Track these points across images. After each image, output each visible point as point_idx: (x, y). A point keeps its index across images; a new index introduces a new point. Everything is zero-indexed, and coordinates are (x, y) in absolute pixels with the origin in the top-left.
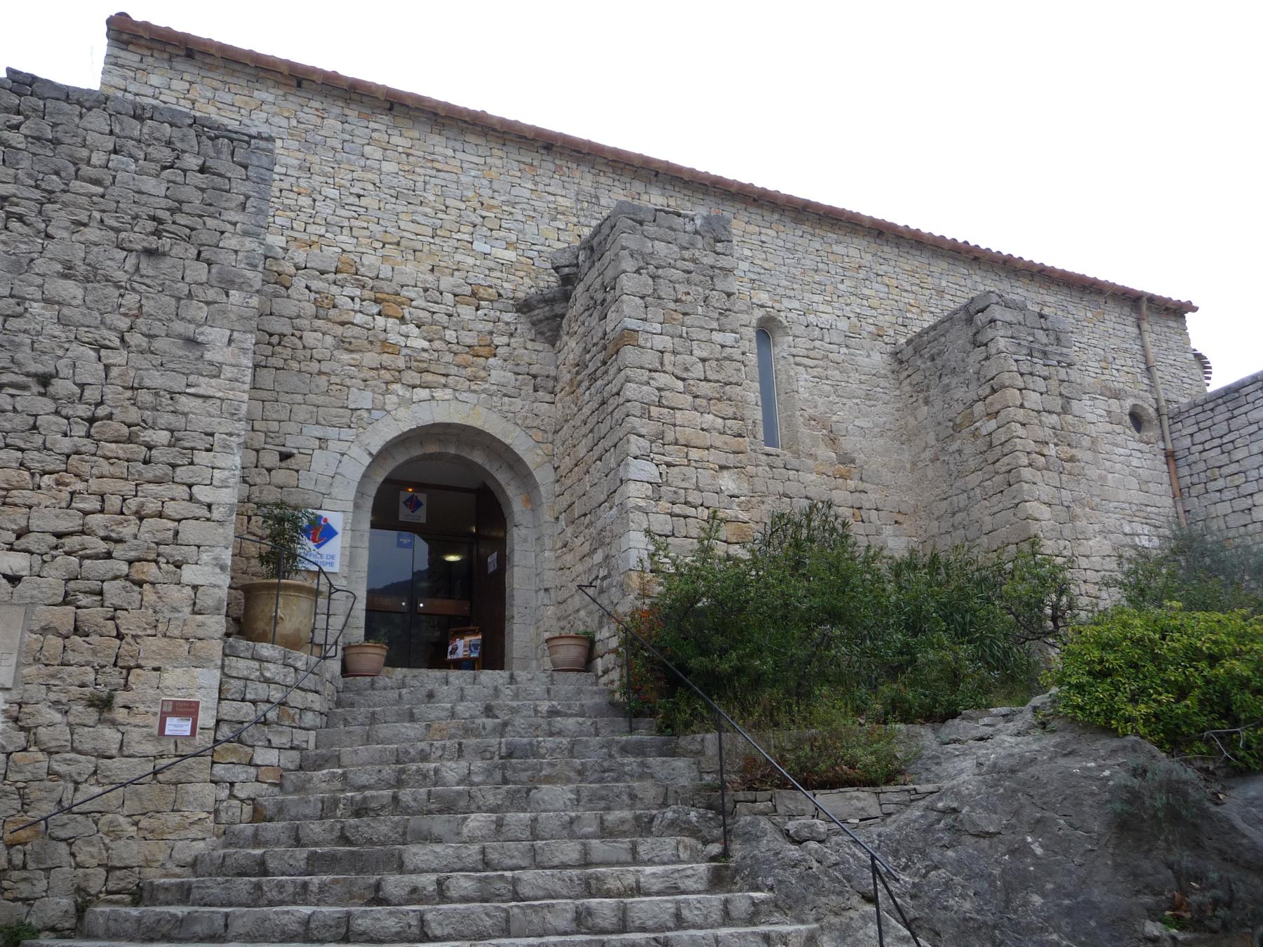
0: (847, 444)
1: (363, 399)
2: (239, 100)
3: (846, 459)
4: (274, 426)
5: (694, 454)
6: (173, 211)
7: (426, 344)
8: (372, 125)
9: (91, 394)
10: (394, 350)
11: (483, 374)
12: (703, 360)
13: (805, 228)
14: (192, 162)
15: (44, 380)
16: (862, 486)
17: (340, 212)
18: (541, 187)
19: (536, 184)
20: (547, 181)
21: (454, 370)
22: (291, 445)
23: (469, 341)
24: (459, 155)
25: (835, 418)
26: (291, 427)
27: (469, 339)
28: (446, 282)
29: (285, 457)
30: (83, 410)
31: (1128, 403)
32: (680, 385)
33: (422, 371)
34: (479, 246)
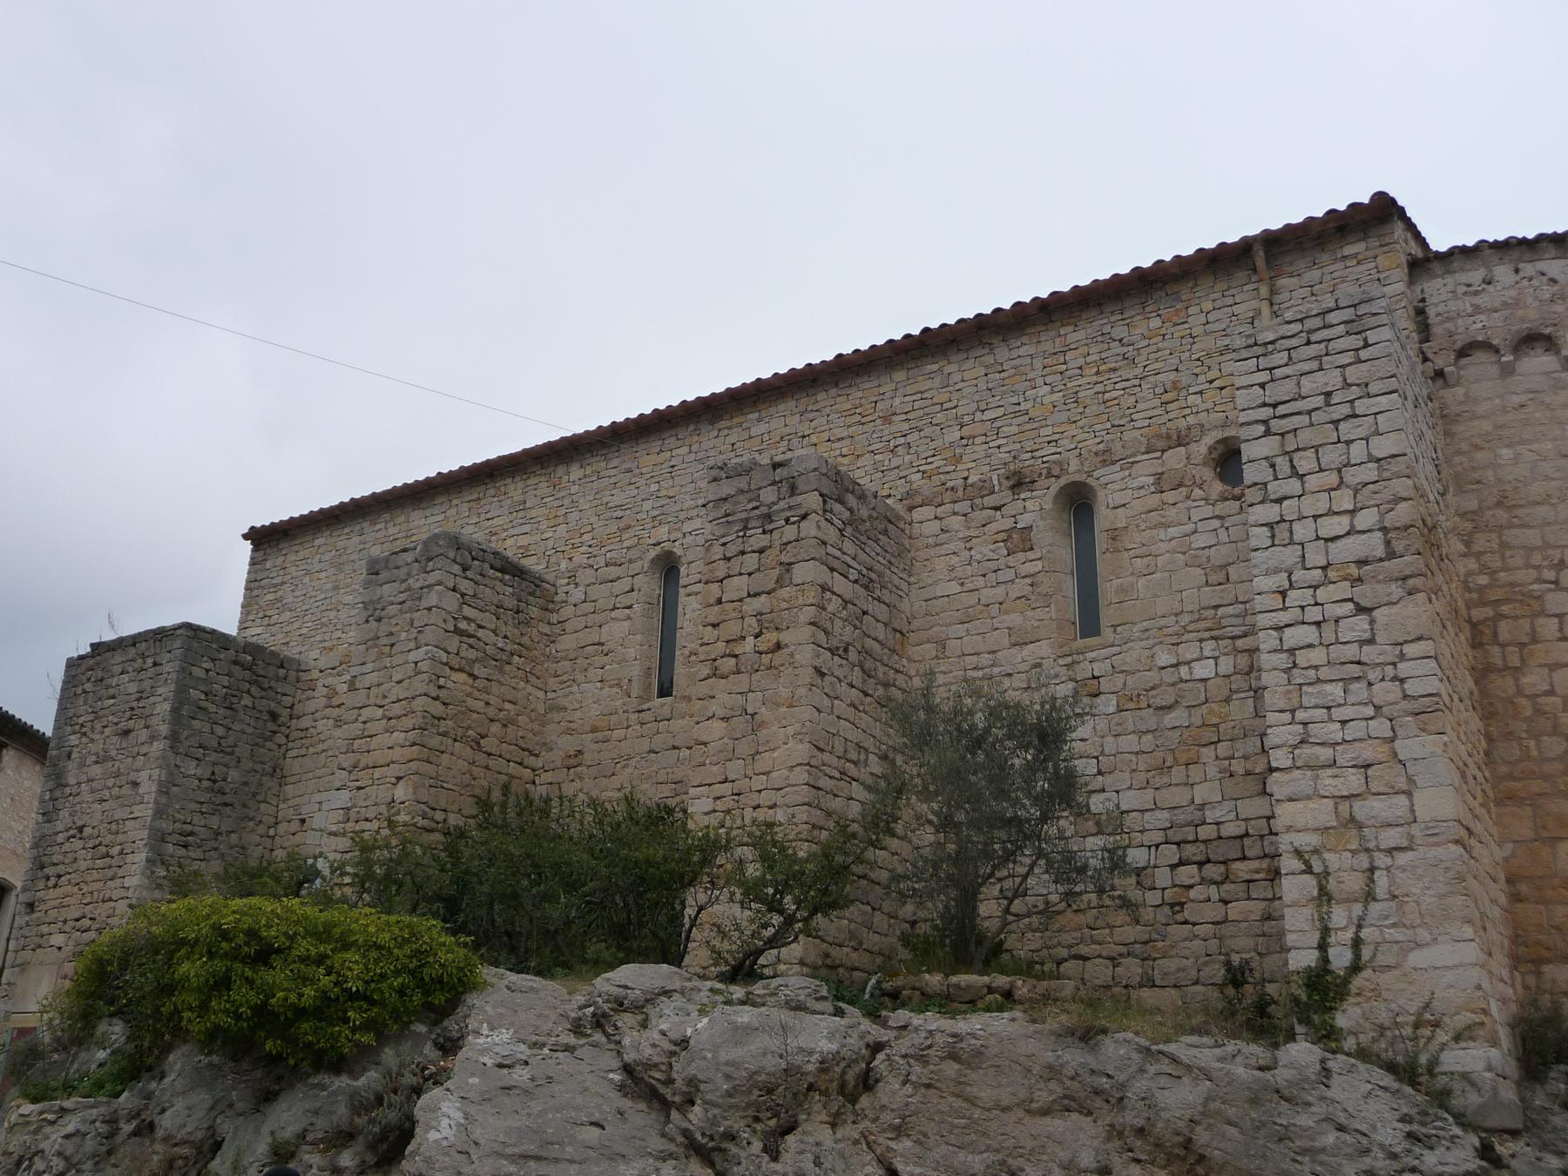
6: (138, 700)
8: (378, 526)
14: (150, 661)
26: (305, 799)
31: (1201, 448)
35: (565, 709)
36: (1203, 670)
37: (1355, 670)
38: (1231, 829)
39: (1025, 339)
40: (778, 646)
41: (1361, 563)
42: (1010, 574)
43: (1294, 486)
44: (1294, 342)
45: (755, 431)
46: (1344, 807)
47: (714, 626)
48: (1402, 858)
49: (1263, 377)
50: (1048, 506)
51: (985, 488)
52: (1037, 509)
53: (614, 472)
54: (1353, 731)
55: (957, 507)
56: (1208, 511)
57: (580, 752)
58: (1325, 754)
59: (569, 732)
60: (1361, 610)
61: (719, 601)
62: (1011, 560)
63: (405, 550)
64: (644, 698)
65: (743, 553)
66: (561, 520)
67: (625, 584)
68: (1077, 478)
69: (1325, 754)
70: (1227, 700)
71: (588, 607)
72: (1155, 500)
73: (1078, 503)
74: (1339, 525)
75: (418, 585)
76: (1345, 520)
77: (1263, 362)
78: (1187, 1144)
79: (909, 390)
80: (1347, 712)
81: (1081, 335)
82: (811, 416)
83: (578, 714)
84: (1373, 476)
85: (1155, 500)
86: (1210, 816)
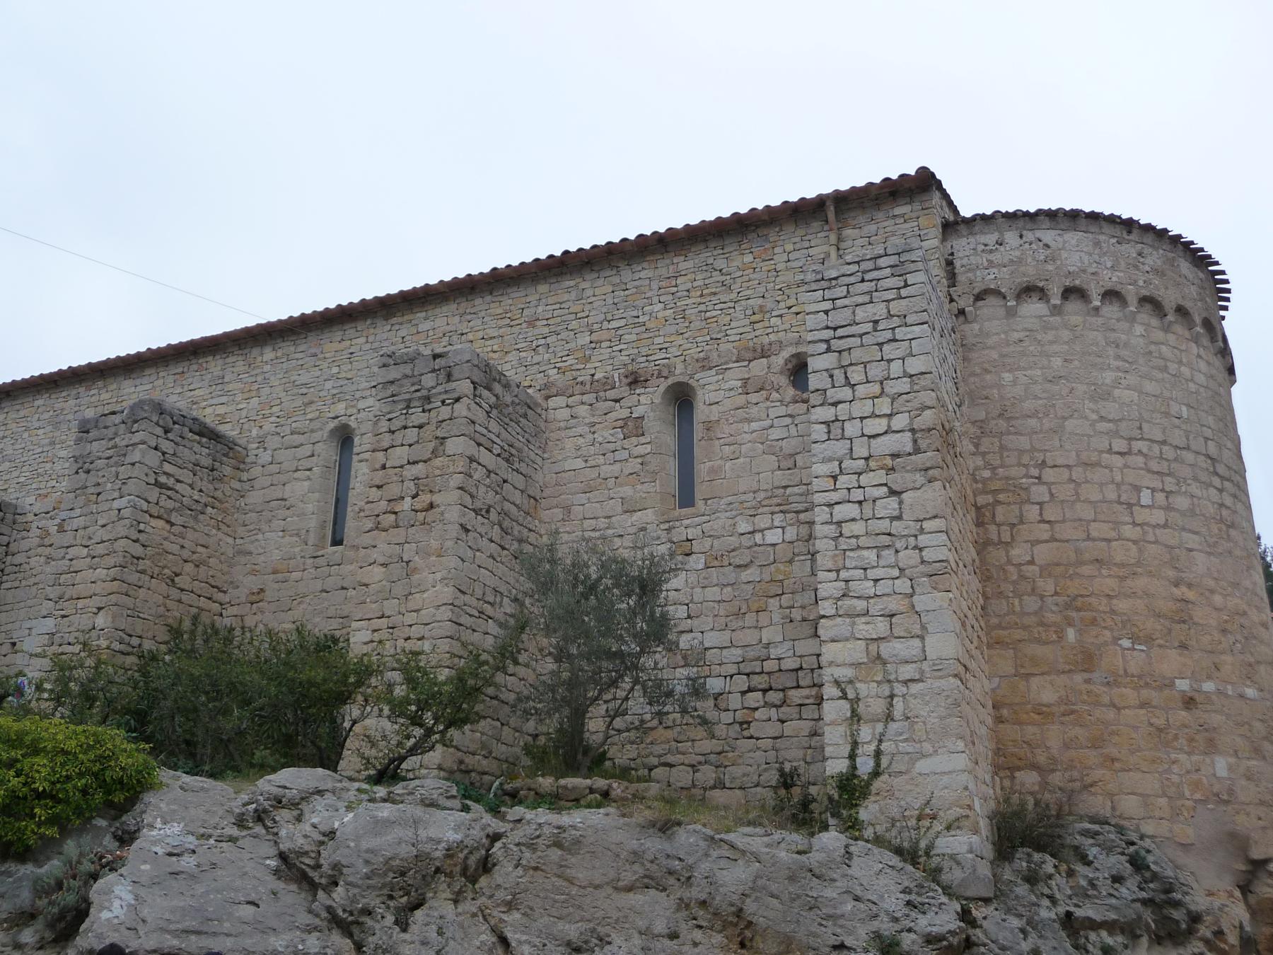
5: (81, 604)
22: (15, 636)
29: (14, 644)
31: (779, 361)
35: (251, 553)
36: (773, 537)
38: (790, 664)
39: (645, 265)
41: (895, 456)
42: (625, 454)
43: (846, 393)
44: (852, 280)
46: (873, 647)
47: (379, 487)
48: (915, 688)
49: (827, 305)
51: (608, 384)
52: (649, 402)
53: (300, 355)
54: (883, 588)
56: (782, 411)
58: (861, 605)
59: (254, 572)
60: (893, 493)
63: (114, 413)
65: (405, 428)
66: (254, 394)
67: (307, 450)
68: (681, 379)
69: (861, 605)
70: (791, 562)
73: (682, 399)
75: (124, 443)
76: (884, 421)
77: (828, 294)
79: (550, 301)
81: (690, 264)
82: (469, 317)
83: (262, 558)
84: (907, 388)
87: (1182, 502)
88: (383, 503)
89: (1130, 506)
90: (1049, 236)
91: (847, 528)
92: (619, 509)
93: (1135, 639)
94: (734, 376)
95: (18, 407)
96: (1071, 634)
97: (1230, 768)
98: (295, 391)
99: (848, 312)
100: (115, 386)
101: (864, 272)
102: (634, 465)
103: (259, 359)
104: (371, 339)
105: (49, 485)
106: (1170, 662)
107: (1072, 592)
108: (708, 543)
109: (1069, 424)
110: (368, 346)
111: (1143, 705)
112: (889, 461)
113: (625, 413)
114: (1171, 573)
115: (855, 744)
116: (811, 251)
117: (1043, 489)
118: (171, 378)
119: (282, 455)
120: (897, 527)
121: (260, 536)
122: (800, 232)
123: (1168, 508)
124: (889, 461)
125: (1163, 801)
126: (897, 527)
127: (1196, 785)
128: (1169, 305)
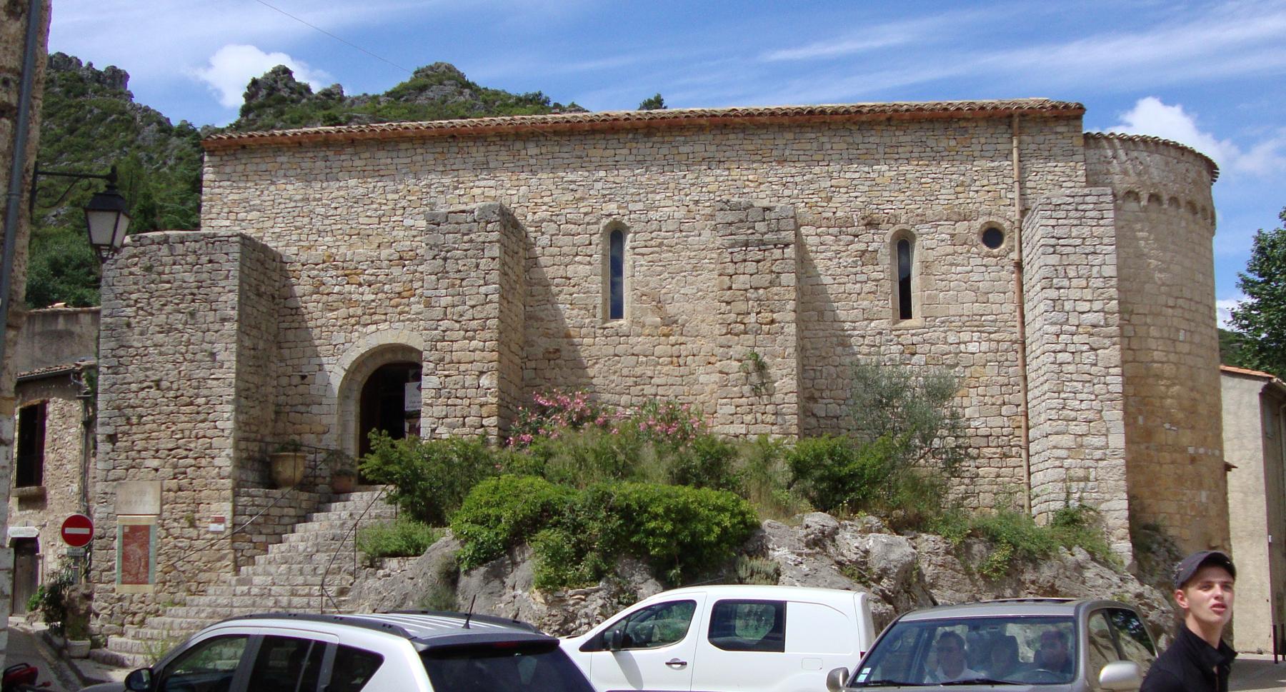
0: (671, 309)
1: (339, 337)
2: (270, 166)
3: (669, 321)
4: (296, 362)
5: (462, 367)
6: (198, 288)
7: (373, 297)
8: (343, 157)
9: (175, 386)
10: (357, 303)
11: (407, 309)
12: (473, 307)
13: (655, 139)
14: (204, 259)
15: (158, 384)
16: (683, 339)
17: (326, 222)
18: (448, 167)
19: (445, 166)
20: (452, 161)
21: (390, 310)
22: (305, 370)
23: (398, 290)
24: (396, 161)
25: (663, 291)
26: (305, 361)
27: (398, 287)
28: (385, 253)
29: (303, 377)
30: (172, 394)
31: (978, 224)
32: (457, 325)
33: (369, 315)
34: (408, 222)
35: (542, 320)
36: (972, 347)
37: (1087, 377)
38: (982, 431)
39: (873, 132)
40: (773, 322)
41: (1094, 326)
42: (864, 277)
43: (1066, 283)
44: (1070, 207)
45: (682, 149)
46: (1079, 439)
47: (728, 303)
48: (1102, 464)
49: (1053, 222)
50: (888, 240)
51: (847, 222)
52: (881, 241)
53: (566, 155)
54: (1084, 406)
55: (831, 230)
56: (979, 261)
57: (557, 351)
58: (1073, 414)
59: (547, 335)
60: (1092, 349)
61: (730, 288)
62: (865, 269)
63: (463, 212)
64: (605, 320)
65: (745, 261)
66: (523, 183)
67: (584, 238)
68: (905, 227)
69: (1073, 414)
70: (985, 366)
71: (555, 250)
72: (950, 249)
73: (904, 244)
74: (1086, 306)
75: (481, 239)
76: (1088, 304)
77: (1054, 215)
78: (1052, 586)
79: (795, 146)
80: (1084, 396)
81: (908, 138)
82: (725, 148)
83: (553, 325)
84: (1101, 285)
85: (950, 249)
86: (973, 424)
87: (1197, 339)
88: (733, 316)
89: (1174, 341)
90: (1144, 156)
91: (1066, 368)
92: (861, 317)
93: (1172, 423)
94: (945, 230)
95: (258, 160)
96: (1141, 420)
97: (1208, 498)
98: (565, 186)
99: (1066, 229)
100: (367, 155)
101: (1078, 204)
102: (870, 286)
103: (523, 152)
104: (634, 151)
105: (311, 237)
106: (1186, 438)
107: (1144, 394)
108: (927, 347)
109: (1147, 287)
110: (632, 158)
111: (1173, 463)
112: (1090, 329)
113: (862, 246)
114: (1190, 384)
115: (1068, 493)
116: (999, 147)
117: (1130, 328)
118: (430, 157)
119: (562, 240)
120: (1094, 370)
121: (549, 306)
122: (991, 131)
123: (1191, 343)
124: (1090, 329)
125: (1178, 516)
126: (1094, 370)
127: (1193, 507)
128: (1199, 206)
